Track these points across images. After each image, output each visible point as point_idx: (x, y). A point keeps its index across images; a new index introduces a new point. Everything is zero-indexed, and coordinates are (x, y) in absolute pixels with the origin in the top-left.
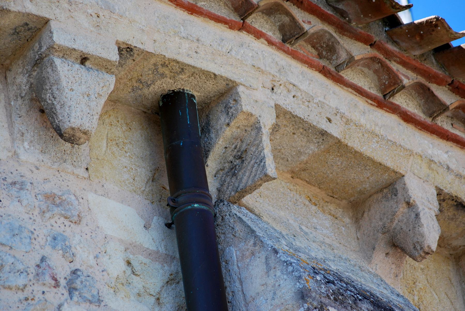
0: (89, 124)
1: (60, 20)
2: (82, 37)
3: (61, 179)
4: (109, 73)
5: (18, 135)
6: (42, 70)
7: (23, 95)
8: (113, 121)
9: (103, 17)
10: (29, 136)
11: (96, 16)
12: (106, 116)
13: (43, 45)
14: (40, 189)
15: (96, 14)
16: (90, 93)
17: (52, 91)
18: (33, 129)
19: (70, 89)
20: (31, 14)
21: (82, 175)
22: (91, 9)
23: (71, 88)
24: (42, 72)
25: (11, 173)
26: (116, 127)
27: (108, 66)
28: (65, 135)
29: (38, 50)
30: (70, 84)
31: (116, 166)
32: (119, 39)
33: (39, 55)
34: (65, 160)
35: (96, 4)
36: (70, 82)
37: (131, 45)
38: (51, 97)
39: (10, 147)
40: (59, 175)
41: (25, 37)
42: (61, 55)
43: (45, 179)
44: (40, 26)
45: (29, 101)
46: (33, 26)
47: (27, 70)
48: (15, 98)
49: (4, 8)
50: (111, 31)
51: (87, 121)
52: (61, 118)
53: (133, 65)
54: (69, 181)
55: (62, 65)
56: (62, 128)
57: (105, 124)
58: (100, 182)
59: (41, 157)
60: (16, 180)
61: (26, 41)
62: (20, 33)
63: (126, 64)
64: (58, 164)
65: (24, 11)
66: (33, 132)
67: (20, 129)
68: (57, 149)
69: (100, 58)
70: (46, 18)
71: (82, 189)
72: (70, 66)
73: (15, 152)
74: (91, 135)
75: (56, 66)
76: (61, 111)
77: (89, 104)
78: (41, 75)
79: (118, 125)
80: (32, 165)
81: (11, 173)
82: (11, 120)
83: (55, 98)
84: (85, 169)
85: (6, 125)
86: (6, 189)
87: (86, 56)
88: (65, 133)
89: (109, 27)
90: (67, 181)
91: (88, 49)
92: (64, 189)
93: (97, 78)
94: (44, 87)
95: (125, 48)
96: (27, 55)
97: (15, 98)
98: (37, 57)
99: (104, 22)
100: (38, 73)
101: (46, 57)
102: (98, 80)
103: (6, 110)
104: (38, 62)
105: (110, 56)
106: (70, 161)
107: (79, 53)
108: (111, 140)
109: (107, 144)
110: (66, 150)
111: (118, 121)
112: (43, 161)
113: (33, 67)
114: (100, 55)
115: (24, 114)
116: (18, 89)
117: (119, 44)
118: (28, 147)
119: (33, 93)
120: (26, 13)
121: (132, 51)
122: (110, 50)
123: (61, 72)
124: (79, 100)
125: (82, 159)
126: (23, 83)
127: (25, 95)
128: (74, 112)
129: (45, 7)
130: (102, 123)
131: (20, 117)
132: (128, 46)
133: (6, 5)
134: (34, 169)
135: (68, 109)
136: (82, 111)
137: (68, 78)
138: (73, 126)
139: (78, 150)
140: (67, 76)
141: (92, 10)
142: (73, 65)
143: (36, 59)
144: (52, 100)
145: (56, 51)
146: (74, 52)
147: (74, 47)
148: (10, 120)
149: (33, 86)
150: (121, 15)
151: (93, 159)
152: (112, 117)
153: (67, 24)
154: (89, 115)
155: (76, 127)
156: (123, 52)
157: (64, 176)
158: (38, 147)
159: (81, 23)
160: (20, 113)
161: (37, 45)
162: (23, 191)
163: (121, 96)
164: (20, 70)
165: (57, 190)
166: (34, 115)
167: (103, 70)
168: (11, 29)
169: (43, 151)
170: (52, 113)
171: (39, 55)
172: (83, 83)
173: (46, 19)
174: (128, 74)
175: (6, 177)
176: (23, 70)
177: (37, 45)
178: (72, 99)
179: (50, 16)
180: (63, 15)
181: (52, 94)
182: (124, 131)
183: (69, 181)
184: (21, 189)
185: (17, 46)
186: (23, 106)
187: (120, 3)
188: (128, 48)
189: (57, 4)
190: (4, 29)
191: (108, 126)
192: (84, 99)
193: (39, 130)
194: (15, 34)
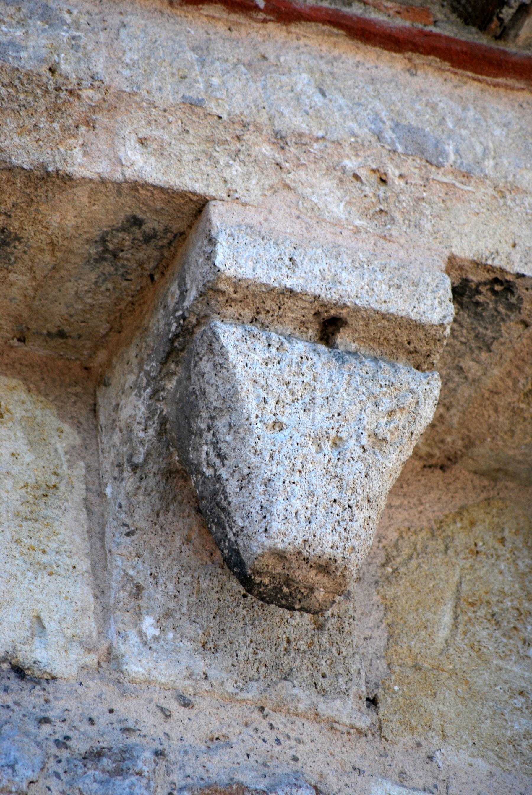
0: (336, 538)
1: (243, 199)
2: (320, 251)
3: (271, 736)
4: (425, 367)
5: (122, 594)
6: (190, 370)
7: (139, 459)
8: (483, 540)
9: (399, 183)
10: (159, 597)
11: (374, 178)
12: (459, 525)
13: (188, 287)
14: (189, 771)
15: (374, 171)
16: (343, 435)
17: (213, 435)
18: (175, 571)
19: (270, 422)
20: (142, 186)
21: (347, 721)
22: (357, 155)
23: (274, 419)
24: (189, 378)
25: (91, 721)
26: (493, 561)
27: (417, 344)
28: (258, 580)
29: (177, 303)
30: (271, 405)
31: (486, 689)
32: (456, 251)
33: (178, 319)
34: (287, 669)
35: (373, 139)
36: (272, 402)
37: (502, 270)
38: (212, 455)
39: (94, 634)
40: (265, 722)
41: (141, 265)
42: (248, 313)
43: (212, 740)
44: (177, 226)
45: (158, 478)
46: (159, 227)
47: (147, 374)
48: (116, 474)
49: (50, 169)
50: (428, 226)
51: (330, 526)
52: (240, 523)
53: (525, 341)
54: (300, 741)
55: (243, 347)
56: (245, 556)
57: (451, 552)
58: (419, 745)
59: (202, 664)
60: (105, 745)
61: (146, 281)
62: (121, 254)
63: (502, 340)
64: (262, 685)
65: (118, 176)
66: (174, 580)
67: (131, 572)
68: (258, 637)
69: (384, 316)
70: (194, 194)
71: (349, 768)
72: (274, 350)
73: (109, 651)
74: (347, 573)
75: (223, 350)
76: (241, 499)
77: (339, 470)
78: (186, 388)
79: (500, 552)
80: (167, 693)
81: (91, 721)
82: (103, 547)
83: (222, 457)
84: (363, 705)
85: (85, 565)
86: (63, 776)
87: (333, 312)
88: (260, 574)
89: (422, 213)
90: (293, 743)
91: (340, 287)
92: (279, 771)
93: (370, 384)
94: (194, 425)
95: (485, 284)
96: (150, 325)
97: (116, 474)
98: (173, 328)
99: (402, 197)
100: (179, 382)
101: (199, 324)
102: (372, 390)
103: (90, 512)
104: (176, 344)
105: (422, 308)
106: (306, 674)
107: (308, 305)
108: (472, 604)
109: (456, 618)
110: (292, 639)
111: (503, 540)
112: (206, 678)
113: (164, 363)
114: (383, 308)
115: (143, 524)
116: (124, 442)
117: (461, 268)
118: (157, 632)
119: (171, 449)
120: (126, 182)
121: (512, 293)
122: (422, 288)
123: (239, 368)
124: (300, 460)
125: (354, 668)
126: (138, 419)
127: (145, 461)
128: (281, 499)
129: (191, 157)
130: (442, 548)
131: (128, 534)
132: (491, 276)
133: (57, 158)
134: (174, 706)
135: (261, 489)
136: (312, 494)
137: (266, 387)
138: (280, 546)
139: (338, 638)
140: (263, 382)
141: (360, 160)
142: (287, 345)
143: (170, 335)
144: (213, 466)
145: (230, 301)
146: (290, 303)
147: (288, 283)
148: (98, 545)
149: (168, 426)
150: (464, 170)
151: (397, 669)
152: (479, 528)
153: (270, 212)
154: (337, 508)
155: (290, 548)
156: (480, 298)
157: (281, 726)
158: (190, 630)
159: (321, 205)
160: (128, 521)
161: (174, 288)
162: (124, 779)
163: (511, 453)
164: (132, 378)
165: (254, 774)
166: (180, 525)
167: (403, 357)
168: (88, 241)
169: (211, 645)
170: (217, 510)
171: (178, 319)
172: (319, 401)
173: (195, 198)
174: (515, 373)
175: (70, 734)
176: (138, 377)
177: (174, 288)
178: (276, 456)
179: (208, 186)
180: (254, 181)
181: (215, 444)
182: (524, 574)
183: (300, 741)
184: (120, 772)
185: (122, 299)
186: (141, 498)
187: (464, 132)
188: (496, 281)
189: (235, 146)
190: (66, 243)
191: (462, 556)
192: (321, 456)
193: (196, 574)
194: (105, 259)
